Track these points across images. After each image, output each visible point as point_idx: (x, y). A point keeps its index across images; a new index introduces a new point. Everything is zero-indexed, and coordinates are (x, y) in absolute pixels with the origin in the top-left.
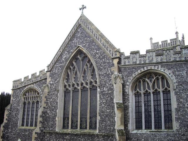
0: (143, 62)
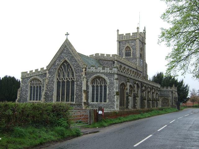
0: (96, 72)
